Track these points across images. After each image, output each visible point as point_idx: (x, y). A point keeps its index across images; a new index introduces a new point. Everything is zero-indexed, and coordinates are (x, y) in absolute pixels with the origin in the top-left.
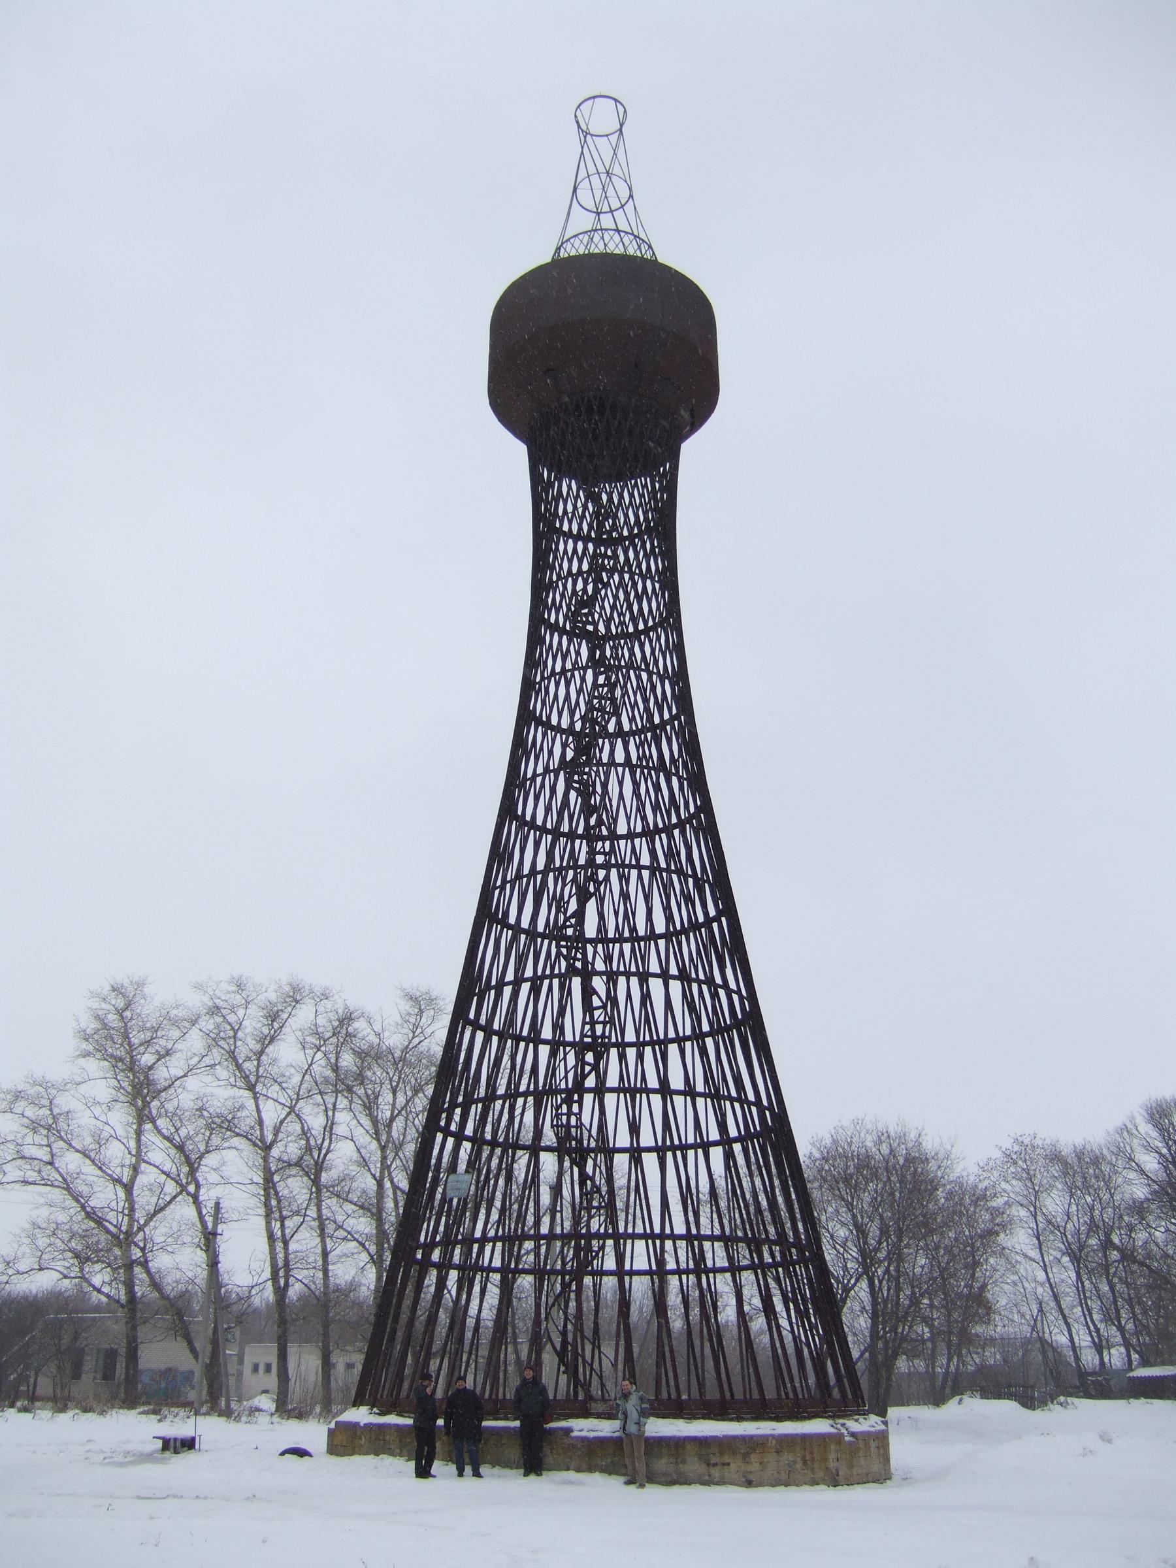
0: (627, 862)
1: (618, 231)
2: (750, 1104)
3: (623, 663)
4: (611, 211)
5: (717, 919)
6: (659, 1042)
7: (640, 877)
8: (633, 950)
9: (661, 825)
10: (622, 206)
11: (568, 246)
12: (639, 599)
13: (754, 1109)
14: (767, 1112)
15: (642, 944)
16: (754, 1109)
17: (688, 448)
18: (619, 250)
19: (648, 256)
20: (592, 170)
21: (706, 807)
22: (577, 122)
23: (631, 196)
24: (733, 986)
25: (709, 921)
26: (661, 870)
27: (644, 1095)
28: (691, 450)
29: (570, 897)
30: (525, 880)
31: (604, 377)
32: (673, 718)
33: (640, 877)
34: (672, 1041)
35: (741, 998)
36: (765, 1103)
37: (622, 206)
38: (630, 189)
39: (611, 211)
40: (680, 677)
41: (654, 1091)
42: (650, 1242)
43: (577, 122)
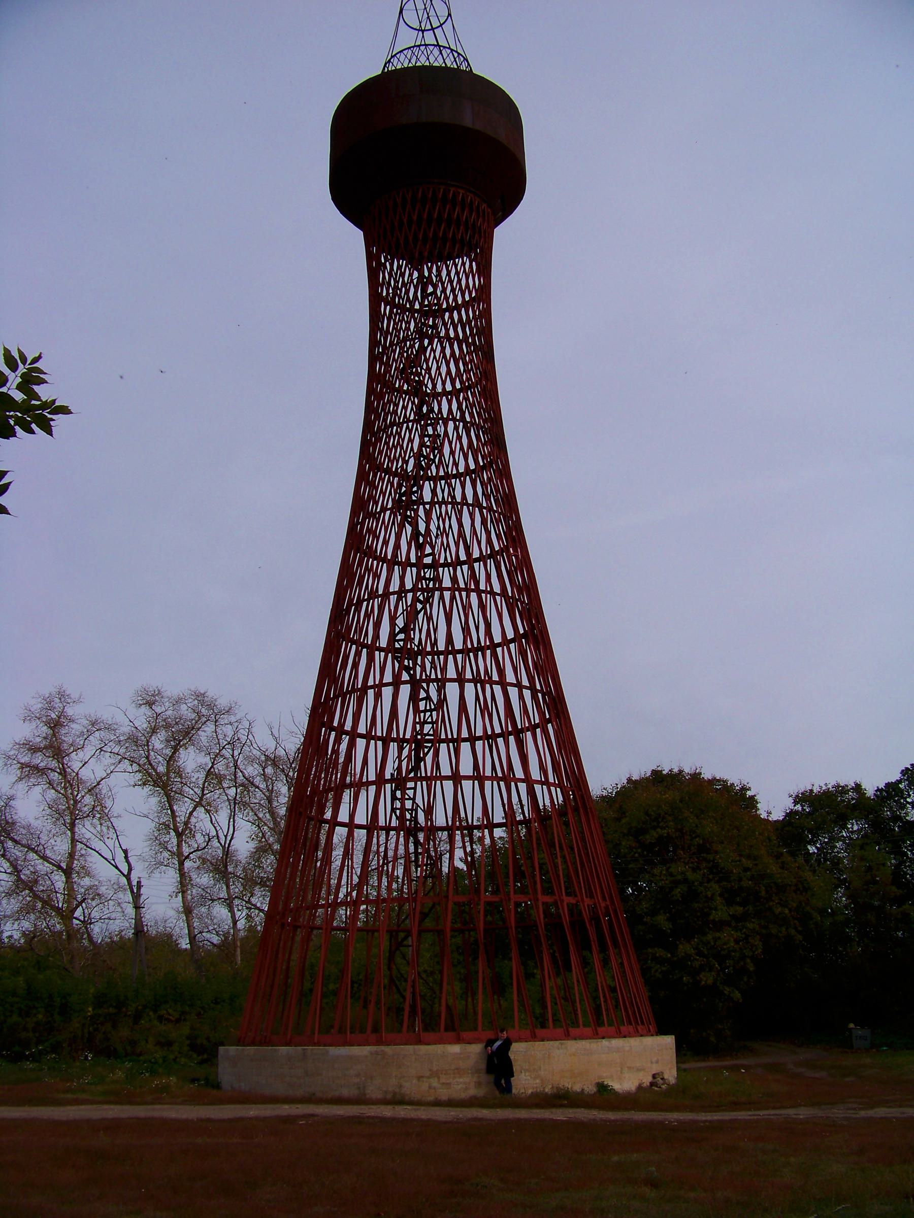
1: (438, 45)
4: (433, 29)
6: (453, 740)
7: (442, 597)
8: (433, 662)
11: (395, 61)
15: (442, 657)
17: (498, 232)
18: (439, 63)
19: (463, 67)
23: (449, 15)
26: (460, 590)
27: (438, 782)
28: (505, 236)
29: (410, 457)
31: (426, 167)
33: (442, 597)
34: (465, 740)
37: (441, 25)
38: (449, 9)
39: (433, 29)
41: (447, 778)
42: (495, 783)
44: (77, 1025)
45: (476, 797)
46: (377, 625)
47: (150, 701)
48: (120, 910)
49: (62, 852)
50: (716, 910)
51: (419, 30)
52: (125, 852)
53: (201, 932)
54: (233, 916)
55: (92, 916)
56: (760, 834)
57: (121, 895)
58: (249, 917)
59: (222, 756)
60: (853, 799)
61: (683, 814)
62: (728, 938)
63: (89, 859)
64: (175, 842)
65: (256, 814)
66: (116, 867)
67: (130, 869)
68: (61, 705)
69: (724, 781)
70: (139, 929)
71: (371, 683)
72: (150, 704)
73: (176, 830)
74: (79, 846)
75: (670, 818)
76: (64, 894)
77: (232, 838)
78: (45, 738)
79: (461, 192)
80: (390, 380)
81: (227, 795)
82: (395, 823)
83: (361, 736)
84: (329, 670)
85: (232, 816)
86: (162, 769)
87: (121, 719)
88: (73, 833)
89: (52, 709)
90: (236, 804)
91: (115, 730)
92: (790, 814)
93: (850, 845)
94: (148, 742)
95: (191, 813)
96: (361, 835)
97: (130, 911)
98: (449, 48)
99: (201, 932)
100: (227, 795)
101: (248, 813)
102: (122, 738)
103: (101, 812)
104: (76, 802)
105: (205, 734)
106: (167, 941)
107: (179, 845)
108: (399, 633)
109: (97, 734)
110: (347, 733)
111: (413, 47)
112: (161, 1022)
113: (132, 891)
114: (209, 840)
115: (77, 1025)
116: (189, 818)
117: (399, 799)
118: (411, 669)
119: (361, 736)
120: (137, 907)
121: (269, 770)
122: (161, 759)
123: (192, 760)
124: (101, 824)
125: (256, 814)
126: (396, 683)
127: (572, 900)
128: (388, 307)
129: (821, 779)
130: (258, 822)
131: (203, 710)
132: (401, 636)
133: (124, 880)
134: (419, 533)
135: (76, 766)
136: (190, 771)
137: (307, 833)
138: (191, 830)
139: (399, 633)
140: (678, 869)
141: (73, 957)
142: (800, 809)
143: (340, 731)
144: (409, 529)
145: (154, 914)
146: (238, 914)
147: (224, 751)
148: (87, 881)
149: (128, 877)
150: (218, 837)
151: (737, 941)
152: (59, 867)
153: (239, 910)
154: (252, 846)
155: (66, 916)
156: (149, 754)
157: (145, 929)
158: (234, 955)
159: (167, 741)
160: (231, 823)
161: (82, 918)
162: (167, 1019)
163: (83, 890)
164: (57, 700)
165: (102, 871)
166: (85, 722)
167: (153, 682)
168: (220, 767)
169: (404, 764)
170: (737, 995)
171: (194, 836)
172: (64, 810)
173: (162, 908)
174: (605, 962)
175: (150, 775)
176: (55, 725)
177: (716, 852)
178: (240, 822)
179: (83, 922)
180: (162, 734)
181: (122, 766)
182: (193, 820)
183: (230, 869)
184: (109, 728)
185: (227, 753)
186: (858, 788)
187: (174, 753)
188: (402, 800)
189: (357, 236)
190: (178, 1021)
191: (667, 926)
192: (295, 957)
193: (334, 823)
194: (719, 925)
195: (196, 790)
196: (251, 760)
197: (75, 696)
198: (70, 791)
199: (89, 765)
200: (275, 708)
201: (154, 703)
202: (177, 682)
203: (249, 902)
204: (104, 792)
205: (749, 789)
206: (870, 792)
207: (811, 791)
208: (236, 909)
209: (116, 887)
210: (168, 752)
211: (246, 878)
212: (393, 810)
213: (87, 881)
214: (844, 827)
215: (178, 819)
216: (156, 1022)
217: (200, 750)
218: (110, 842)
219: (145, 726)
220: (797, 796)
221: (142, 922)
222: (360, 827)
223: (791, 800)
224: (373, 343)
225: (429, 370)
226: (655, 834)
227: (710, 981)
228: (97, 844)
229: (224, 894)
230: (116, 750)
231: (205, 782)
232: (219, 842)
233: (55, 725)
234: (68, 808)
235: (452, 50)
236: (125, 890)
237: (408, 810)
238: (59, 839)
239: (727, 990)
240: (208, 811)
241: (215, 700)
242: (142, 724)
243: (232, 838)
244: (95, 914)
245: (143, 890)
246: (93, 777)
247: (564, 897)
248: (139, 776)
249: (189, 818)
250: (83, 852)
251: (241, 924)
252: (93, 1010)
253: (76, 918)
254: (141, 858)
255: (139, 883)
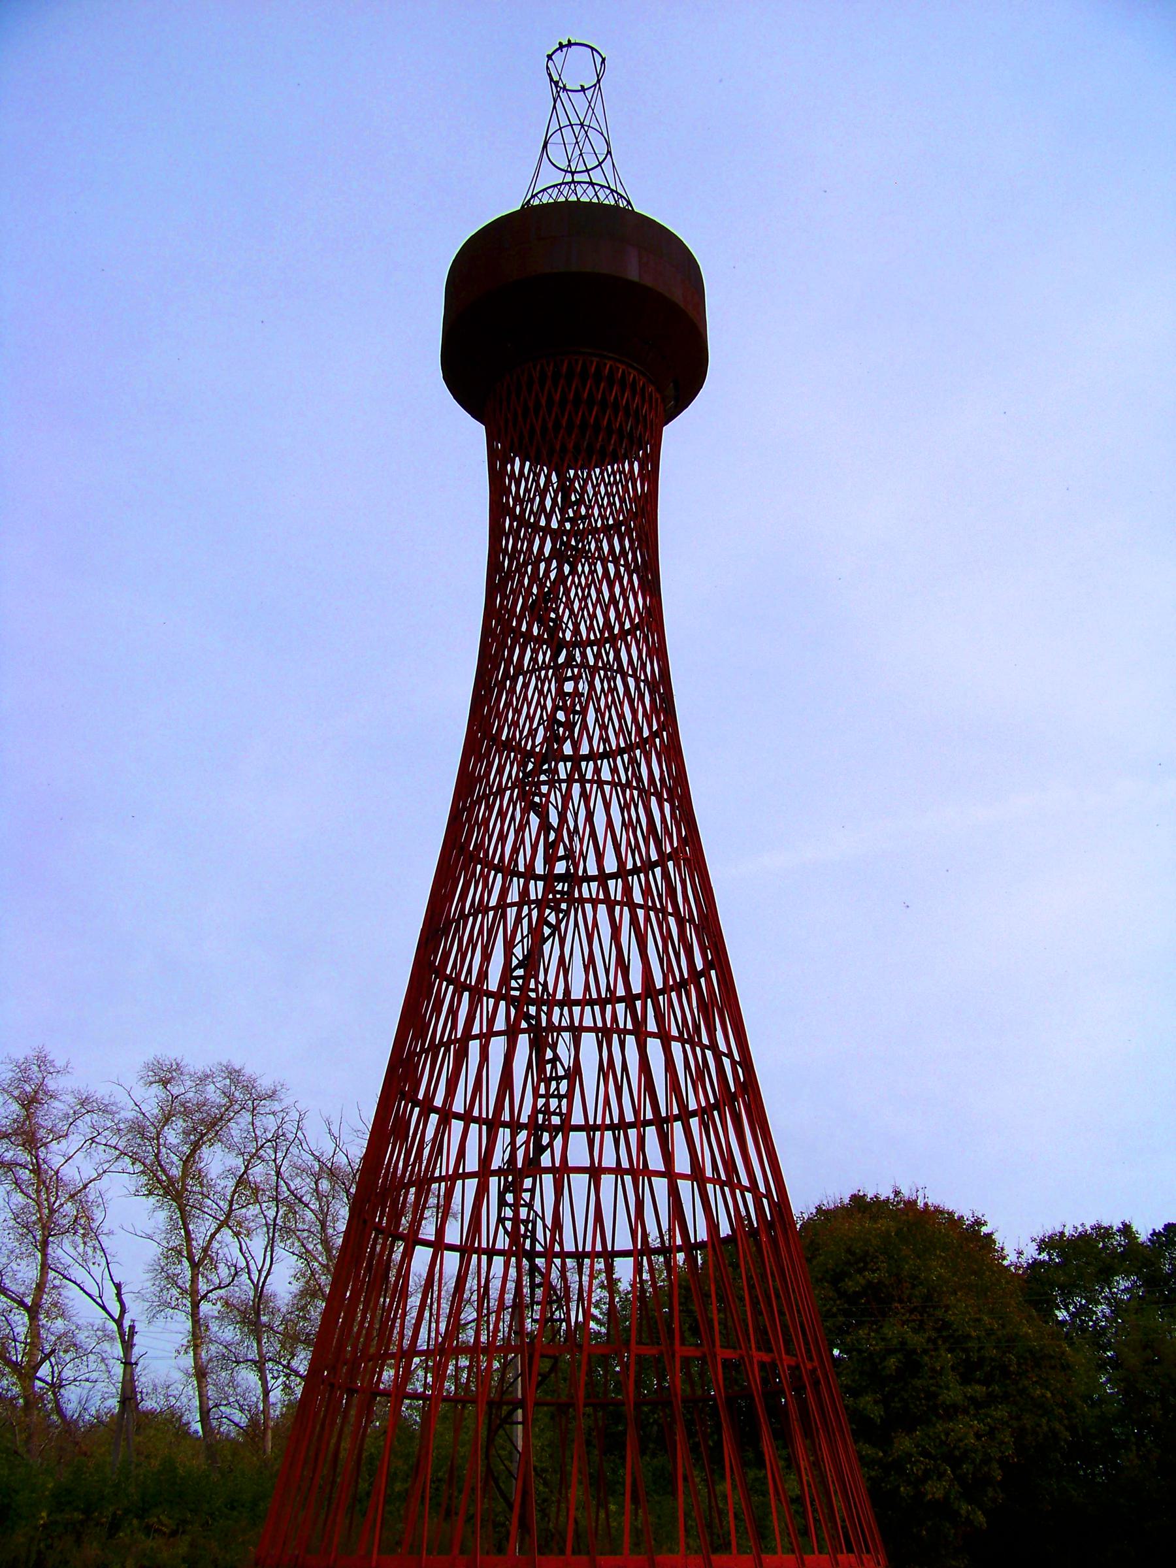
0: (595, 786)
2: (743, 1189)
3: (602, 673)
5: (705, 973)
9: (623, 745)
10: (600, 164)
12: (613, 600)
13: (748, 1195)
14: (765, 1201)
16: (748, 1195)
17: (670, 432)
20: (564, 122)
21: (692, 838)
22: (550, 75)
23: (609, 152)
24: (723, 1047)
25: (695, 975)
28: (676, 436)
30: (491, 913)
31: (574, 339)
32: (654, 735)
35: (734, 1063)
36: (763, 1189)
37: (600, 164)
38: (608, 144)
40: (661, 687)
43: (550, 75)
44: (22, 1540)
45: (611, 1218)
46: (487, 957)
47: (165, 1076)
48: (103, 1367)
49: (28, 1281)
50: (948, 1388)
51: (566, 171)
52: (118, 1286)
53: (217, 1406)
54: (263, 1379)
55: (64, 1375)
56: (1007, 1283)
57: (106, 1346)
58: (286, 1387)
59: (259, 1158)
60: (1120, 1245)
61: (902, 1254)
62: (965, 1429)
63: (64, 1292)
64: (188, 1274)
65: (303, 1245)
66: (104, 1308)
67: (123, 1311)
68: (40, 1075)
69: (948, 1213)
70: (129, 1395)
71: (476, 1030)
72: (165, 1083)
73: (190, 1258)
74: (52, 1274)
75: (882, 1258)
76: (26, 1344)
77: (268, 1274)
78: (15, 1121)
79: (621, 367)
80: (516, 618)
81: (265, 1217)
82: (502, 1242)
83: (458, 1116)
84: (413, 1018)
85: (271, 1243)
86: (176, 1172)
87: (122, 1098)
88: (45, 1255)
89: (27, 1080)
90: (277, 1231)
91: (113, 1113)
92: (1035, 1264)
93: (1117, 1307)
94: (158, 1133)
95: (213, 1236)
96: (452, 1261)
97: (119, 1369)
98: (609, 188)
99: (217, 1406)
100: (265, 1217)
101: (293, 1244)
102: (122, 1126)
103: (86, 1227)
104: (52, 1211)
105: (237, 1128)
106: (172, 1420)
107: (194, 1280)
108: (517, 967)
109: (87, 1117)
110: (436, 1110)
111: (561, 184)
112: (148, 1535)
113: (123, 1341)
114: (236, 1273)
115: (22, 1540)
116: (210, 1242)
117: (510, 1205)
118: (532, 1017)
119: (458, 1116)
120: (128, 1364)
121: (325, 1185)
122: (175, 1159)
123: (217, 1162)
124: (85, 1243)
125: (303, 1245)
126: (511, 1034)
127: (766, 1358)
128: (528, 464)
129: (1075, 1217)
130: (306, 1255)
131: (237, 1094)
132: (520, 972)
133: (114, 1326)
134: (550, 827)
135: (56, 1161)
136: (214, 1177)
137: (373, 1248)
138: (212, 1259)
139: (517, 967)
140: (893, 1330)
141: (30, 1437)
142: (1047, 1258)
143: (427, 1107)
144: (534, 820)
145: (152, 1376)
146: (271, 1382)
147: (262, 1152)
148: (59, 1325)
149: (119, 1322)
150: (249, 1273)
151: (978, 1436)
152: (22, 1303)
153: (273, 1378)
154: (296, 1287)
155: (26, 1374)
156: (159, 1152)
157: (139, 1396)
158: (264, 1438)
159: (188, 1136)
160: (269, 1253)
161: (49, 1379)
162: (158, 1531)
163: (53, 1338)
164: (36, 1068)
165: (83, 1312)
166: (71, 1099)
167: (170, 1054)
168: (259, 1173)
169: (520, 1154)
170: (980, 1518)
171: (216, 1268)
172: (35, 1223)
173: (164, 1364)
174: (791, 1462)
175: (160, 1181)
176: (30, 1102)
177: (947, 1308)
178: (279, 1251)
179: (53, 1385)
180: (180, 1124)
181: (119, 1165)
182: (215, 1245)
183: (264, 1319)
184: (105, 1110)
185: (267, 1153)
186: (1126, 1229)
187: (193, 1151)
188: (516, 1207)
189: (478, 430)
190: (174, 1533)
191: (876, 1412)
192: (345, 1444)
193: (413, 1240)
194: (952, 1411)
195: (222, 1203)
196: (301, 1170)
197: (60, 1063)
198: (45, 1196)
199: (72, 1160)
200: (333, 1101)
201: (169, 1082)
202: (201, 1051)
203: (288, 1366)
204: (91, 1198)
205: (985, 1224)
206: (1143, 1236)
207: (1062, 1233)
208: (269, 1376)
209: (100, 1333)
210: (186, 1149)
211: (285, 1334)
212: (501, 1220)
213: (59, 1325)
214: (1109, 1283)
215: (194, 1243)
216: (141, 1536)
217: (230, 1148)
218: (96, 1271)
219: (156, 1111)
220: (1043, 1241)
221: (135, 1388)
222: (452, 1248)
223: (1034, 1246)
224: (494, 566)
225: (569, 604)
226: (862, 1281)
227: (939, 1494)
228: (78, 1273)
229: (253, 1355)
230: (113, 1142)
231: (234, 1192)
232: (250, 1278)
233: (30, 1102)
234: (40, 1219)
235: (612, 191)
236: (113, 1339)
237: (523, 1221)
238: (24, 1263)
239: (965, 1508)
240: (237, 1234)
241: (255, 1081)
242: (152, 1109)
243: (268, 1274)
244: (68, 1373)
245: (136, 1339)
246: (77, 1177)
247: (754, 1352)
248: (144, 1179)
249: (210, 1242)
250: (57, 1282)
251: (276, 1395)
252: (48, 1516)
253: (40, 1379)
254: (139, 1295)
255: (132, 1327)
